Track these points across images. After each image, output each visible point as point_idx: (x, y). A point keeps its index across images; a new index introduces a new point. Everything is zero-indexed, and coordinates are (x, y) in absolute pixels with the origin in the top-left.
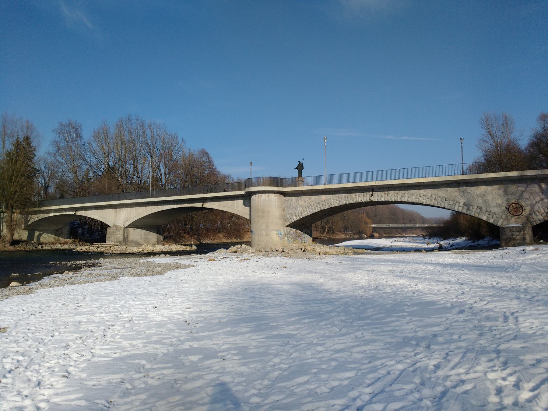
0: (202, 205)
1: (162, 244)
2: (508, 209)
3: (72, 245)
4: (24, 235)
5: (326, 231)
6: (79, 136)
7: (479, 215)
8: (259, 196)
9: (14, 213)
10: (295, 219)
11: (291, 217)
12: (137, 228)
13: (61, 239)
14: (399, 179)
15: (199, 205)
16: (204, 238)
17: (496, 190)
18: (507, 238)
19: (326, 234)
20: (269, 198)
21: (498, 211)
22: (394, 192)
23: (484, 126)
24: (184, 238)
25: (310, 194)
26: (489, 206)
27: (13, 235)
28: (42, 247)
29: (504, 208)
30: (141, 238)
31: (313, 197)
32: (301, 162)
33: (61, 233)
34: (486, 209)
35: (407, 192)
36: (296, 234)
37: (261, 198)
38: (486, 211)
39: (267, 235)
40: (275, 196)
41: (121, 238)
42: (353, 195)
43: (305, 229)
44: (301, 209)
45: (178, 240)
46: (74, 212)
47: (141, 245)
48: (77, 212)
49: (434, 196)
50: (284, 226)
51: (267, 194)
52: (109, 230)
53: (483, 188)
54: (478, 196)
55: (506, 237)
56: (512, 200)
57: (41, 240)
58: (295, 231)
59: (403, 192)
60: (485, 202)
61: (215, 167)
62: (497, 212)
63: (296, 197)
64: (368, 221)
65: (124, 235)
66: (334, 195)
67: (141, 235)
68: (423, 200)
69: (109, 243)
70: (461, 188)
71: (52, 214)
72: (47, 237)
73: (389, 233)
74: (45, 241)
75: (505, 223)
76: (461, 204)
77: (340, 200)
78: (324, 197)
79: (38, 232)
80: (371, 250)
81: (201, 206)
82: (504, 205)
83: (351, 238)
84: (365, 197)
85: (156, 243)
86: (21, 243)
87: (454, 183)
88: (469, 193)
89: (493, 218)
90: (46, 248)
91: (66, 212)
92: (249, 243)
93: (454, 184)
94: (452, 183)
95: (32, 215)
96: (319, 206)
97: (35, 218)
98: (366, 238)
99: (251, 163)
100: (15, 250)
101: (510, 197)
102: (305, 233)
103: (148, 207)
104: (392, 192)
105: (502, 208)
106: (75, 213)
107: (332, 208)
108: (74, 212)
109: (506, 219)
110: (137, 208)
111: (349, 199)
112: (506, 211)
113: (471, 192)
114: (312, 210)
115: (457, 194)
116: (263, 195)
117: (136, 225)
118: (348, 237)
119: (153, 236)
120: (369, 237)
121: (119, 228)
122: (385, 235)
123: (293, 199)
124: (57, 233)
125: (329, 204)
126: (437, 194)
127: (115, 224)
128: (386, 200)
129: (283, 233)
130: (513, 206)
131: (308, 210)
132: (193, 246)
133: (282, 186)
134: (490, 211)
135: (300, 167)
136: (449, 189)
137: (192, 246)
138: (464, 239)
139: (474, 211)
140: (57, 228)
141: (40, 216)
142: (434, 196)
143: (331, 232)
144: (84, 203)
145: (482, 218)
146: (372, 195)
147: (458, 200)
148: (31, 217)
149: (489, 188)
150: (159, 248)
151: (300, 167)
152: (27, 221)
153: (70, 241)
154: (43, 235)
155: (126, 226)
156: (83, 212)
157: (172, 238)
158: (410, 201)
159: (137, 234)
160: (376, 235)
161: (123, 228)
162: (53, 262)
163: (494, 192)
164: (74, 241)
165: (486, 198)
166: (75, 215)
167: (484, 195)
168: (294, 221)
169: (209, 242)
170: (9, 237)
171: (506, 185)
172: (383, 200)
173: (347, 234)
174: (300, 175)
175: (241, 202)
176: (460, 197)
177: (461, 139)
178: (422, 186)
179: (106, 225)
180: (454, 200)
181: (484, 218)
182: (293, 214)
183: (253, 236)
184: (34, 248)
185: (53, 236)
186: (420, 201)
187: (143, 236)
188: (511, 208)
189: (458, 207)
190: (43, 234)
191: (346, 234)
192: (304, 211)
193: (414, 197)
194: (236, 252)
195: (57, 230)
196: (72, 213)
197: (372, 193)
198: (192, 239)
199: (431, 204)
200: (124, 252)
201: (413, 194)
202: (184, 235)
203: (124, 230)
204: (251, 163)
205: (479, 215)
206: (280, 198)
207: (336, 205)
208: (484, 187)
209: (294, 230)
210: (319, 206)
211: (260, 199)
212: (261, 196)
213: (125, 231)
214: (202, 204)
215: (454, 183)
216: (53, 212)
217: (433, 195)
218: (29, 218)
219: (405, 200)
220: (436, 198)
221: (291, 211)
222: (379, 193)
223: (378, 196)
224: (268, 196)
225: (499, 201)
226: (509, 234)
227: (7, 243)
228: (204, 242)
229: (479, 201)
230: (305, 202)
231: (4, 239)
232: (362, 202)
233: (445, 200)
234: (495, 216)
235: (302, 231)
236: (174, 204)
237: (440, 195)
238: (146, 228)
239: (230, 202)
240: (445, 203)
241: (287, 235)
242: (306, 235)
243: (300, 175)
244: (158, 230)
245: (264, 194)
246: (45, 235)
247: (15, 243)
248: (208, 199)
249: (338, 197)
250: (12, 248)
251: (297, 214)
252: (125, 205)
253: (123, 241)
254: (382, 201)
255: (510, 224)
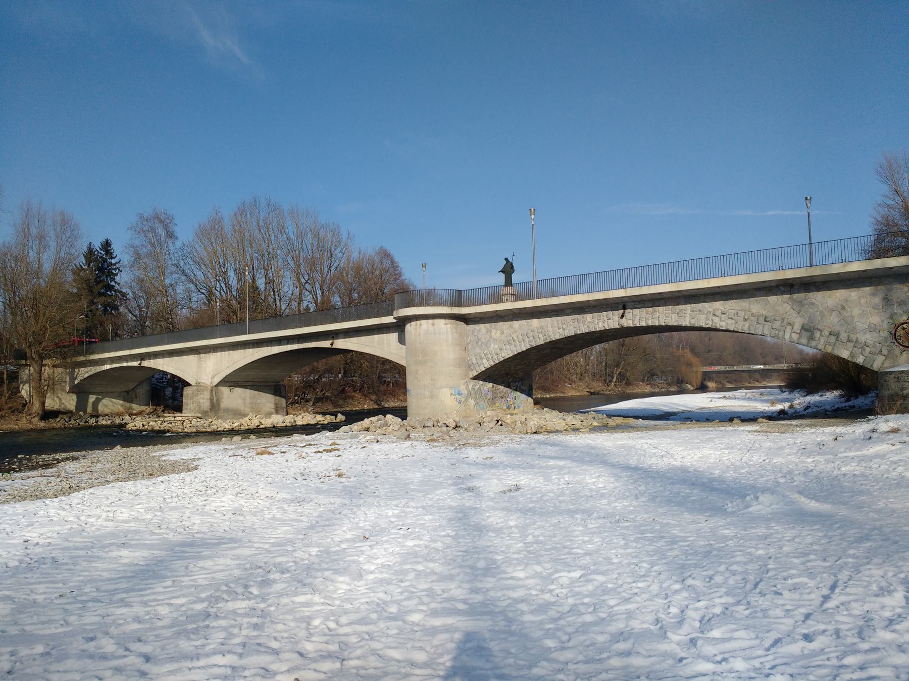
0: (332, 344)
1: (285, 413)
2: (894, 335)
3: (151, 416)
4: (70, 402)
5: (614, 380)
6: (171, 235)
7: (833, 349)
8: (416, 324)
9: (45, 365)
10: (486, 364)
11: (480, 362)
12: (236, 387)
13: (135, 406)
14: (671, 282)
15: (326, 344)
16: (388, 399)
17: (869, 297)
18: (892, 395)
19: (615, 385)
20: (434, 329)
21: (875, 340)
22: (664, 308)
23: (885, 179)
24: (353, 399)
25: (512, 317)
26: (854, 330)
27: (43, 403)
28: (97, 422)
29: (885, 334)
30: (245, 403)
31: (517, 324)
32: (510, 260)
33: (134, 396)
34: (849, 336)
35: (688, 307)
36: (495, 392)
37: (420, 328)
38: (849, 341)
39: (432, 397)
40: (446, 324)
41: (206, 404)
42: (589, 317)
43: (515, 382)
44: (496, 346)
45: (341, 402)
46: (139, 362)
47: (244, 415)
48: (143, 362)
49: (741, 314)
50: (468, 380)
51: (430, 321)
52: (187, 391)
53: (839, 295)
54: (831, 311)
55: (890, 392)
56: (901, 315)
57: (99, 408)
58: (493, 387)
59: (681, 307)
60: (847, 322)
61: (403, 278)
62: (870, 342)
63: (487, 325)
64: (694, 360)
65: (211, 400)
66: (553, 319)
67: (244, 399)
68: (721, 321)
69: (188, 413)
70: (795, 296)
71: (108, 367)
72: (111, 404)
73: (736, 381)
74: (107, 411)
75: (887, 364)
76: (797, 327)
77: (564, 326)
78: (535, 322)
79: (95, 396)
80: (645, 418)
81: (330, 346)
82: (885, 326)
83: (662, 392)
84: (610, 321)
85: (273, 411)
86: (61, 416)
87: (781, 285)
88: (813, 304)
89: (863, 355)
90: (104, 423)
91: (127, 361)
92: (402, 413)
93: (781, 288)
94: (778, 286)
95: (79, 368)
96: (527, 340)
97: (84, 373)
98: (692, 392)
99: (424, 266)
100: (47, 428)
101: (896, 309)
102: (516, 390)
103: (247, 350)
104: (661, 309)
105: (881, 332)
106: (140, 364)
107: (552, 342)
108: (139, 362)
109: (890, 355)
110: (231, 352)
111: (581, 325)
112: (890, 339)
113: (818, 303)
114: (515, 349)
115: (788, 309)
116: (424, 322)
117: (233, 380)
118: (657, 390)
119: (267, 400)
120: (697, 389)
121: (202, 388)
122: (729, 386)
123: (482, 327)
124: (128, 396)
125: (545, 335)
126: (747, 308)
127: (199, 381)
128: (650, 324)
129: (465, 392)
130: (904, 329)
131: (508, 347)
132: (339, 415)
133: (460, 305)
134: (857, 341)
135: (508, 270)
136: (773, 299)
137: (336, 417)
138: (837, 393)
139: (822, 341)
140: (125, 389)
141: (91, 370)
142: (741, 314)
143: (624, 382)
144: (149, 346)
145: (840, 355)
146: (623, 316)
147: (791, 320)
148: (79, 371)
149: (853, 294)
150: (278, 420)
151: (508, 270)
152: (73, 378)
153: (149, 409)
154: (104, 401)
155: (215, 383)
156: (152, 361)
157: (331, 400)
158: (696, 325)
159: (236, 398)
160: (711, 385)
161: (209, 388)
162: (23, 456)
163: (863, 301)
164: (156, 410)
165: (847, 315)
166: (140, 368)
167: (843, 308)
168: (484, 369)
169: (396, 405)
170: (36, 406)
171: (888, 286)
172: (644, 324)
173: (655, 385)
174: (508, 282)
175: (394, 336)
176: (794, 314)
177: (806, 199)
178: (718, 293)
179: (180, 380)
180: (783, 320)
181: (845, 354)
182: (483, 355)
183: (409, 397)
184: (82, 423)
185: (121, 402)
186: (714, 324)
187: (248, 400)
188: (900, 332)
189: (791, 335)
190: (102, 399)
191: (652, 385)
192: (501, 349)
193: (703, 317)
194: (367, 429)
195: (127, 392)
196: (136, 364)
197: (622, 311)
198: (366, 400)
199: (736, 329)
200: (204, 430)
201: (700, 311)
202: (353, 393)
203: (212, 391)
204: (424, 266)
205: (833, 349)
206: (456, 328)
207: (558, 337)
208: (843, 291)
209: (490, 385)
210: (527, 340)
211: (418, 330)
212: (421, 325)
213: (214, 393)
214: (331, 341)
215: (781, 285)
216: (109, 362)
217: (739, 312)
218: (76, 374)
219: (686, 322)
220: (746, 318)
221: (479, 351)
222: (636, 311)
223: (635, 318)
224: (433, 325)
225: (875, 320)
226: (894, 386)
227: (34, 417)
228: (386, 406)
229: (833, 321)
230: (502, 333)
231: (29, 410)
232: (606, 330)
233: (765, 321)
234: (868, 350)
235: (508, 386)
236: (288, 344)
237: (754, 311)
238: (254, 386)
239: (376, 337)
240: (763, 326)
241: (476, 395)
242: (518, 394)
243: (508, 282)
244: (277, 389)
245: (425, 321)
246: (105, 401)
247: (48, 415)
248: (341, 333)
249: (560, 322)
250: (42, 424)
251: (489, 356)
252: (211, 348)
253: (211, 409)
254: (643, 327)
255: (898, 365)
